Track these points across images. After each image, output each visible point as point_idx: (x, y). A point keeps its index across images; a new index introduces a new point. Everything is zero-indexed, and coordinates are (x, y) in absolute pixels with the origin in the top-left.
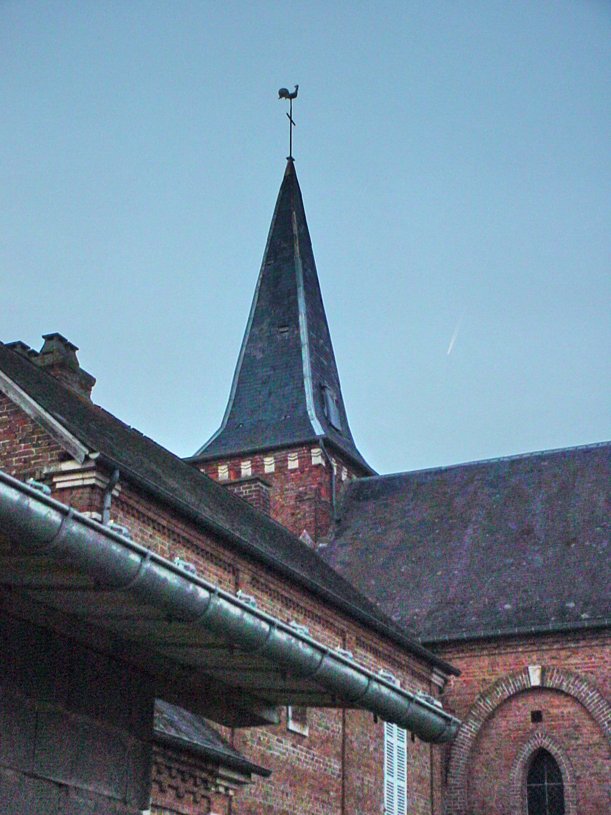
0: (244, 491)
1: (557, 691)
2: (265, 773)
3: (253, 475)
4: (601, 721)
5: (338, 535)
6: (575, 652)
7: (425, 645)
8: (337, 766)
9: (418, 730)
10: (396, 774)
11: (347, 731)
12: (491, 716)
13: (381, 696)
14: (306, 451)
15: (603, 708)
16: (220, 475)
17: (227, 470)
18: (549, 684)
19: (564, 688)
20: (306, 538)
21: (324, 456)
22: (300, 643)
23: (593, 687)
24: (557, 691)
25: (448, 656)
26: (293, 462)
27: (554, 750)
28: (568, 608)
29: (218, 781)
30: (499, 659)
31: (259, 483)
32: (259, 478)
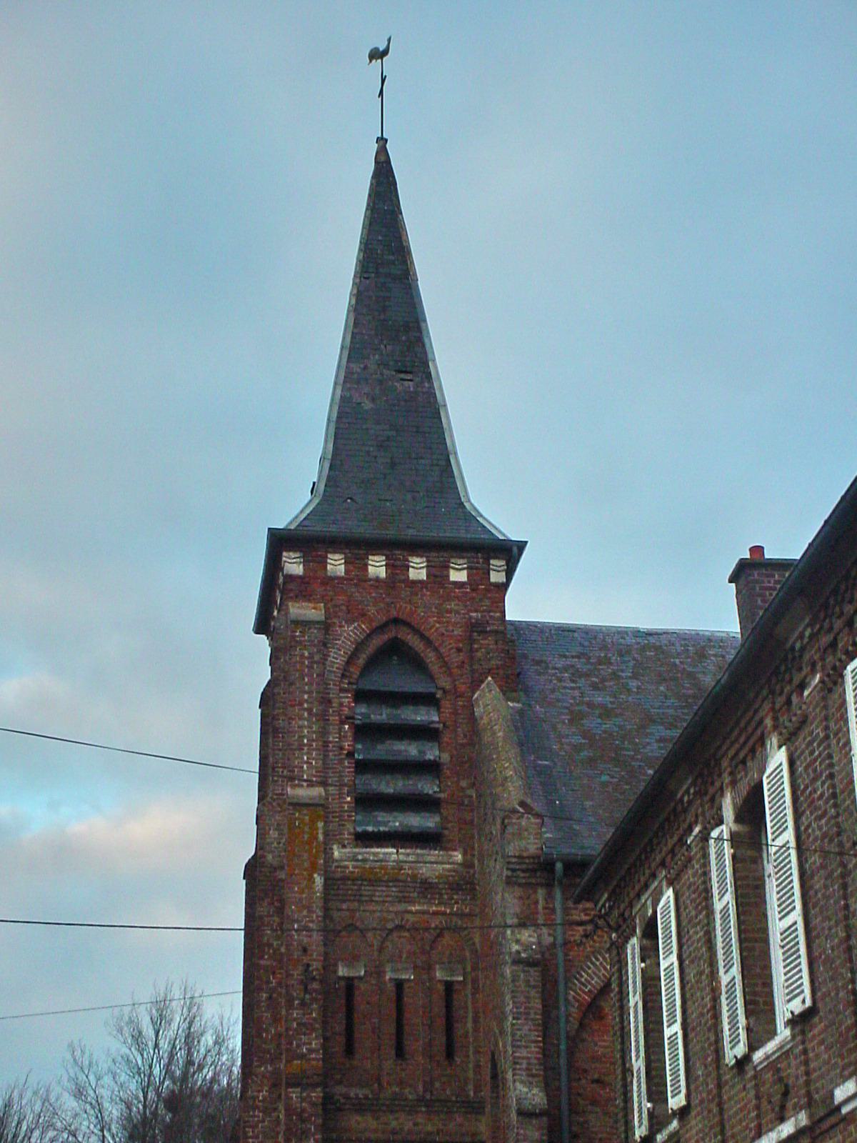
14: (481, 560)
16: (329, 567)
17: (343, 561)
26: (457, 573)
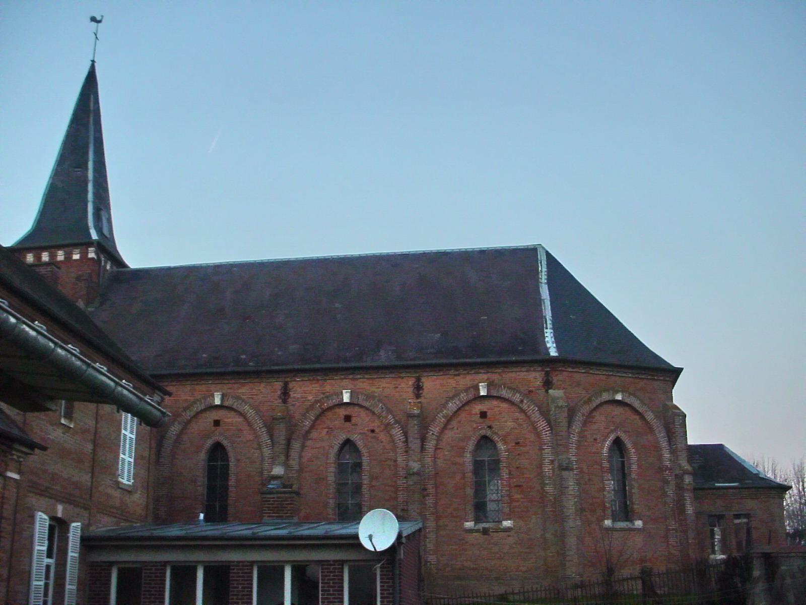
0: (42, 271)
1: (230, 408)
2: (44, 449)
3: (50, 260)
4: (255, 427)
5: (101, 304)
6: (243, 385)
7: (151, 376)
8: (90, 447)
9: (143, 417)
10: (127, 454)
11: (98, 426)
12: (189, 422)
13: (122, 394)
15: (264, 432)
18: (226, 404)
19: (234, 407)
20: (81, 304)
21: (97, 253)
22: (74, 358)
23: (253, 407)
24: (230, 408)
25: (166, 384)
27: (225, 443)
28: (242, 358)
29: (14, 452)
30: (197, 387)
31: (53, 266)
32: (53, 262)
